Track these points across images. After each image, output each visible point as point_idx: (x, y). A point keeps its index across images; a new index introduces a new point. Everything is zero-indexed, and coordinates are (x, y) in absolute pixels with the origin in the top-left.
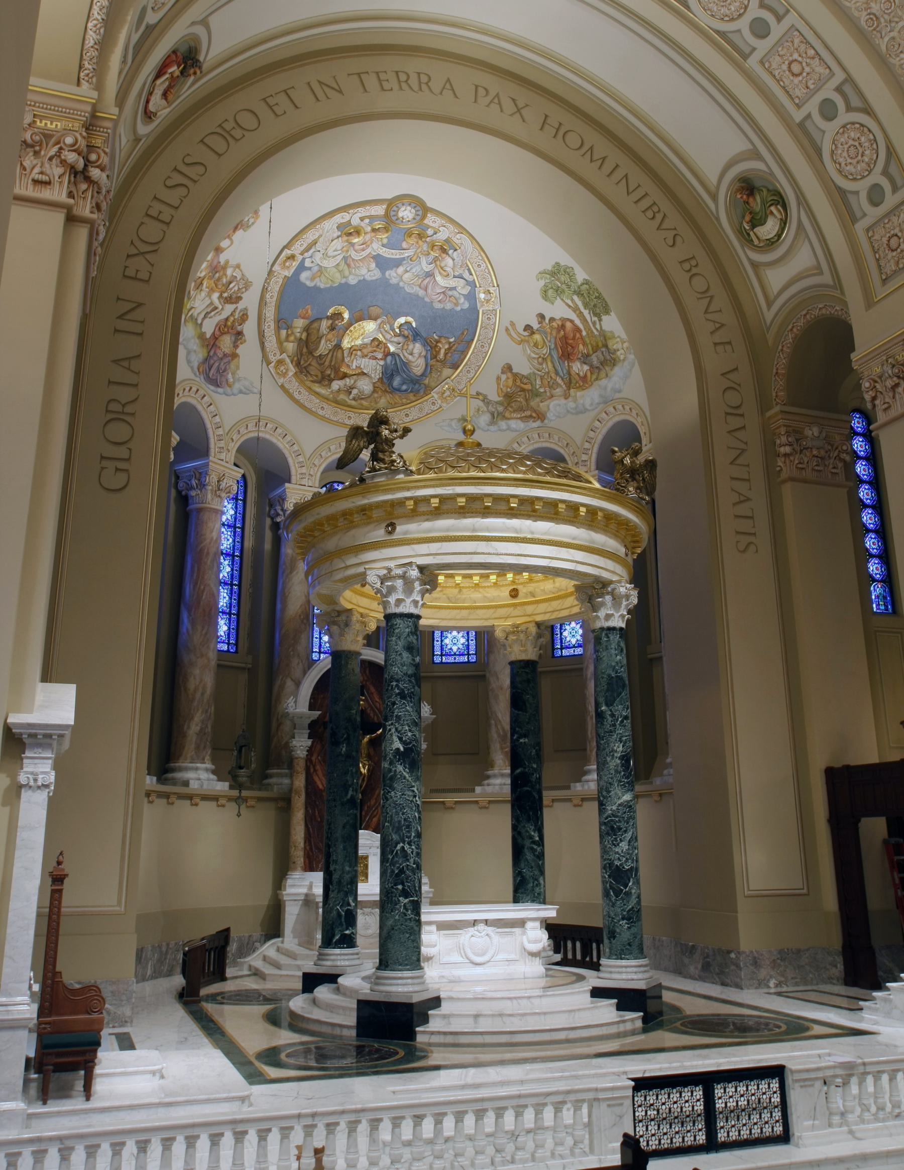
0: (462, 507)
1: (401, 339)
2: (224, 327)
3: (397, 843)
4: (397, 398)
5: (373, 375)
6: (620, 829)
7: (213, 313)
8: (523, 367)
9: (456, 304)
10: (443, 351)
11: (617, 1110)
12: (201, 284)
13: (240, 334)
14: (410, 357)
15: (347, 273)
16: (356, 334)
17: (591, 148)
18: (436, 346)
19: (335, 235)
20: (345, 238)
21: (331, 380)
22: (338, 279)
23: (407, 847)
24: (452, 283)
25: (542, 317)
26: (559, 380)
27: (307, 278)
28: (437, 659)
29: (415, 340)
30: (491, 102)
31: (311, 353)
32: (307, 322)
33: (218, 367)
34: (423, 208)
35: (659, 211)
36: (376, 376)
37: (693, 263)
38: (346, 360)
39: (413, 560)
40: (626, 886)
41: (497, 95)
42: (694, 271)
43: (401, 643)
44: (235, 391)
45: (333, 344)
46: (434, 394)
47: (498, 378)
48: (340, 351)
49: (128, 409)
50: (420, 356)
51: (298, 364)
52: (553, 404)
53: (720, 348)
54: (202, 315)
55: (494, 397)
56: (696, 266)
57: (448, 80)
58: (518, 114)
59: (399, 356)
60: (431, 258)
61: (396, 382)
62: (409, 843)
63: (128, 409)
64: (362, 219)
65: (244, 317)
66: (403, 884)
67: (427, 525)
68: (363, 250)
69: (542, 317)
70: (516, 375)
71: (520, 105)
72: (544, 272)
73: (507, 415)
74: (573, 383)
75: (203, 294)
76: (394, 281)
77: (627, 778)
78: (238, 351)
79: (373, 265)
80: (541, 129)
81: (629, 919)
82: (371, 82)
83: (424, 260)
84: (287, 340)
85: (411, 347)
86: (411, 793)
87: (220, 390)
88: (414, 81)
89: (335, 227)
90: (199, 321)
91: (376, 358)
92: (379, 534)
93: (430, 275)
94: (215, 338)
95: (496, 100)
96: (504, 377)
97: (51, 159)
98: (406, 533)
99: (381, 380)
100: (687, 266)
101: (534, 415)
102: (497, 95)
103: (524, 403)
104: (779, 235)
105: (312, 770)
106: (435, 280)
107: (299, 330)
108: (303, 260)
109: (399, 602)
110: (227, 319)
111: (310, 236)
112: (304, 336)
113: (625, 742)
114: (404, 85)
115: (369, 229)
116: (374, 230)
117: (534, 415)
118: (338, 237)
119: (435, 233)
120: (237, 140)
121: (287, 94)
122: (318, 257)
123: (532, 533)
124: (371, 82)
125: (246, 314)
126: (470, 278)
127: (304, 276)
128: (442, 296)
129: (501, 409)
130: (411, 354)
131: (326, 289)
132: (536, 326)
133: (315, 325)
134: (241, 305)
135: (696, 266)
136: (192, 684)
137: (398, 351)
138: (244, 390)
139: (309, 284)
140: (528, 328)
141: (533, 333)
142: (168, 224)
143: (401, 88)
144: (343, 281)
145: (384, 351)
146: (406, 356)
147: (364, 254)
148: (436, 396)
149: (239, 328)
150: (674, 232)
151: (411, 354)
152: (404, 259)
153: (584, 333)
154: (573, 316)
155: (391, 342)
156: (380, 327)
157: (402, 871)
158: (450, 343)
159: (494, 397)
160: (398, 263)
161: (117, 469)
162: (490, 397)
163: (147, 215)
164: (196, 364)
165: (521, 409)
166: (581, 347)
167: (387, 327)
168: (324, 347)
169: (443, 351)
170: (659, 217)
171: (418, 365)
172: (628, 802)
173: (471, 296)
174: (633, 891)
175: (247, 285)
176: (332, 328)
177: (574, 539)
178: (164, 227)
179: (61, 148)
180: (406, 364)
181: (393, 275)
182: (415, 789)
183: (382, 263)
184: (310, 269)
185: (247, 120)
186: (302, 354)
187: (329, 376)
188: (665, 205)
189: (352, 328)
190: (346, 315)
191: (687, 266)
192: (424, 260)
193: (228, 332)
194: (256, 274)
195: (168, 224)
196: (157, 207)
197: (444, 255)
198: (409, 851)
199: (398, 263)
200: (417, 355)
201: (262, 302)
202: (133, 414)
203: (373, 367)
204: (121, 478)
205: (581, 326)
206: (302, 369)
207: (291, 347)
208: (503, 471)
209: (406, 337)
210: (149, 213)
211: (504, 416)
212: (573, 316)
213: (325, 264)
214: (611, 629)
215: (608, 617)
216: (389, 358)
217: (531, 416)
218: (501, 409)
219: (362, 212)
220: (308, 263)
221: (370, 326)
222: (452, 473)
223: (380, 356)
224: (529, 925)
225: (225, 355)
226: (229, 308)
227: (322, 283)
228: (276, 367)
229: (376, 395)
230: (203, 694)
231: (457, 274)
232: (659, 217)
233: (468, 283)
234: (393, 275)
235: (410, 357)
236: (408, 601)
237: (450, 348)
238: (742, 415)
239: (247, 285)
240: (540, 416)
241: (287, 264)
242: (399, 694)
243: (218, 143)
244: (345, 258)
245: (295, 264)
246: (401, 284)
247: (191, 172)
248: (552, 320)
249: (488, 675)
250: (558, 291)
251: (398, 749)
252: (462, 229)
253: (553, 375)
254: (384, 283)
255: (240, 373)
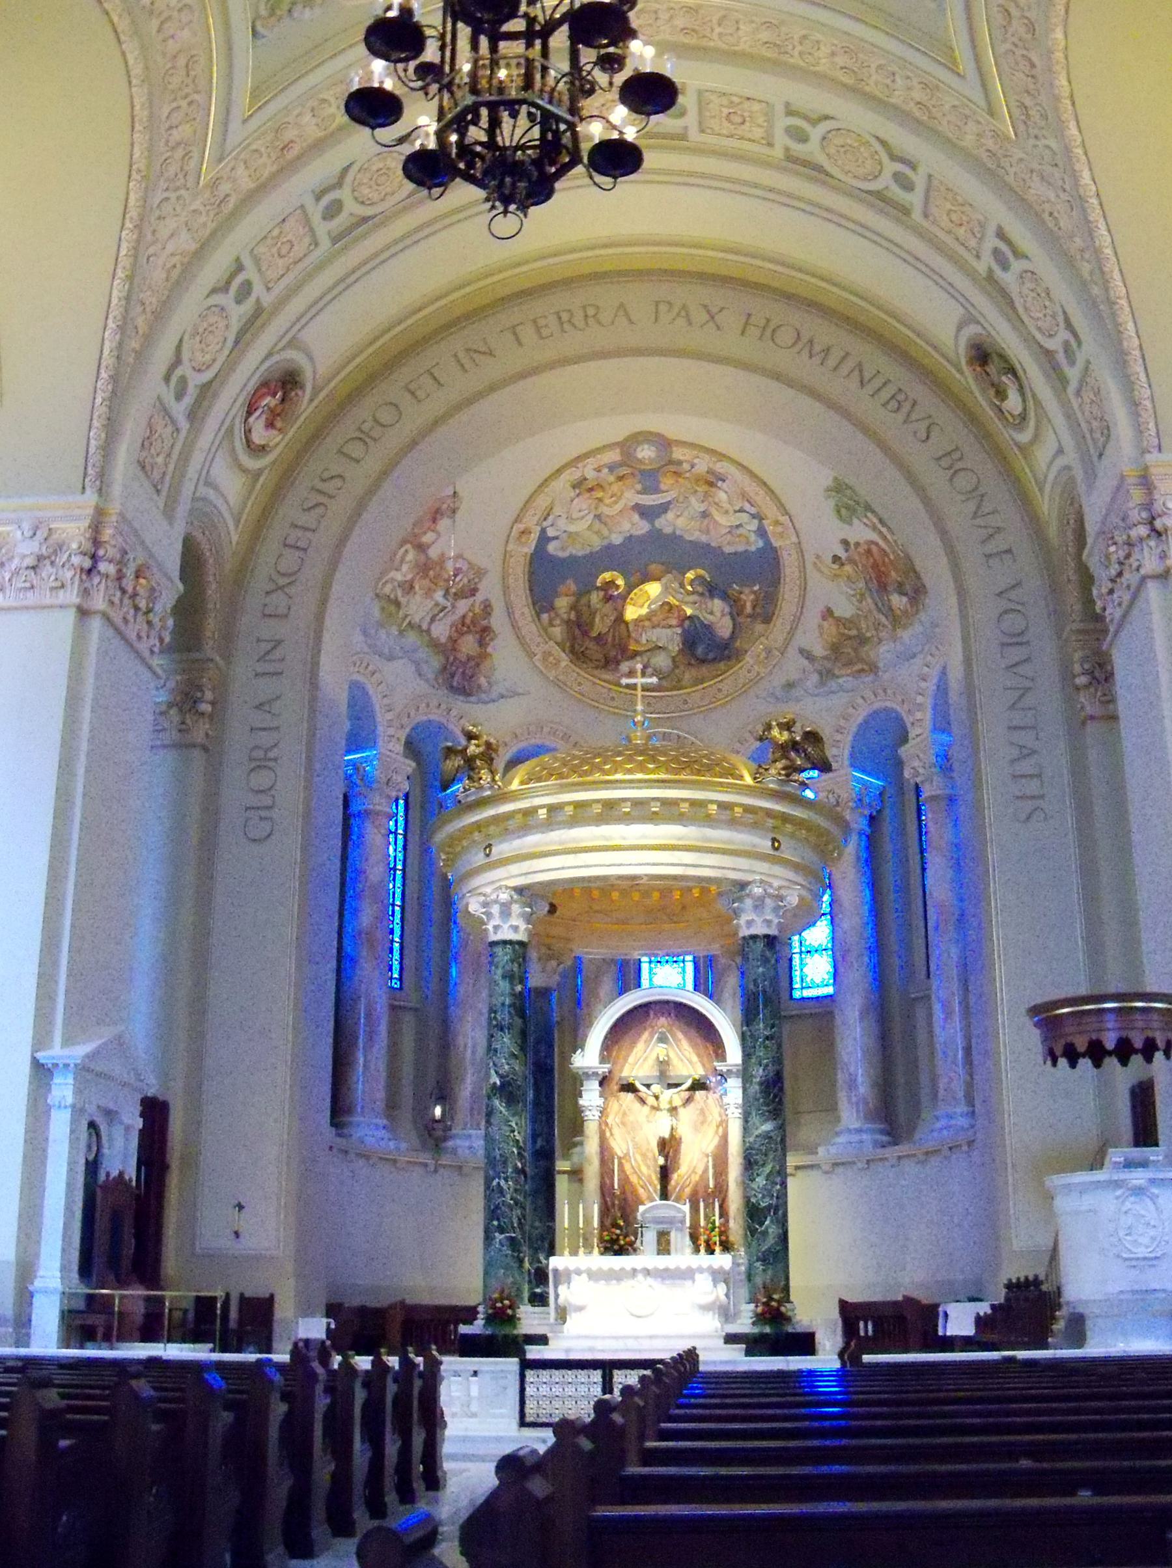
0: (600, 814)
1: (695, 598)
2: (463, 627)
3: (494, 1179)
4: (704, 670)
5: (670, 648)
6: (756, 1163)
7: (441, 615)
8: (845, 609)
9: (748, 543)
10: (749, 605)
11: (502, 1382)
12: (412, 587)
13: (486, 630)
14: (710, 617)
15: (605, 532)
16: (641, 601)
17: (811, 342)
18: (739, 599)
19: (572, 494)
20: (588, 495)
21: (618, 663)
22: (597, 543)
23: (502, 1183)
24: (735, 520)
25: (845, 543)
26: (883, 619)
27: (556, 549)
28: (797, 994)
29: (712, 596)
30: (678, 314)
31: (585, 633)
32: (572, 599)
33: (463, 673)
34: (664, 443)
35: (906, 399)
36: (675, 647)
37: (956, 455)
38: (633, 635)
39: (503, 883)
40: (761, 1224)
41: (684, 307)
42: (959, 465)
43: (500, 972)
44: (494, 695)
45: (612, 618)
46: (748, 659)
47: (820, 626)
48: (623, 626)
49: (271, 755)
50: (723, 615)
51: (573, 651)
52: (883, 649)
53: (994, 562)
54: (428, 619)
55: (819, 651)
56: (960, 459)
57: (622, 305)
58: (711, 324)
59: (698, 618)
60: (700, 495)
61: (700, 650)
62: (506, 1180)
63: (271, 755)
64: (598, 470)
65: (487, 608)
66: (498, 1219)
67: (517, 843)
68: (616, 502)
69: (845, 543)
70: (838, 620)
71: (714, 310)
72: (828, 490)
73: (836, 672)
74: (897, 620)
75: (418, 597)
76: (668, 530)
77: (768, 1105)
78: (489, 650)
79: (636, 517)
80: (743, 333)
81: (764, 1261)
82: (527, 334)
83: (693, 500)
84: (551, 625)
85: (710, 604)
86: (507, 1128)
87: (472, 699)
88: (578, 319)
89: (568, 485)
90: (425, 627)
91: (670, 626)
92: (479, 859)
93: (705, 515)
94: (453, 641)
95: (683, 313)
96: (825, 623)
97: (63, 566)
98: (500, 853)
99: (681, 651)
100: (945, 462)
101: (865, 667)
102: (684, 307)
103: (853, 654)
104: (1025, 409)
105: (608, 1134)
106: (716, 522)
107: (563, 610)
108: (543, 531)
109: (496, 928)
110: (464, 617)
111: (542, 502)
112: (573, 616)
113: (767, 1065)
114: (566, 326)
115: (612, 478)
116: (621, 478)
117: (865, 667)
118: (578, 495)
119: (692, 467)
120: (375, 440)
121: (515, 334)
122: (562, 523)
123: (624, 838)
124: (527, 334)
125: (489, 606)
126: (753, 510)
127: (551, 548)
128: (729, 536)
129: (829, 665)
130: (711, 613)
131: (584, 557)
132: (843, 555)
133: (584, 601)
134: (480, 597)
135: (960, 459)
136: (460, 1041)
137: (697, 613)
138: (505, 693)
139: (561, 554)
140: (836, 559)
141: (842, 564)
142: (305, 550)
143: (563, 331)
144: (605, 543)
145: (679, 616)
146: (707, 618)
147: (619, 507)
148: (751, 662)
149: (484, 623)
150: (926, 423)
151: (711, 613)
152: (669, 503)
153: (892, 557)
154: (874, 536)
155: (686, 603)
156: (666, 589)
157: (497, 1207)
158: (754, 593)
159: (819, 651)
160: (664, 508)
161: (261, 818)
162: (815, 653)
163: (285, 545)
164: (431, 676)
165: (849, 663)
166: (893, 573)
167: (675, 585)
168: (600, 626)
169: (749, 605)
170: (906, 407)
171: (724, 628)
172: (768, 1132)
173: (761, 532)
174: (770, 1231)
175: (480, 573)
176: (608, 599)
177: (679, 839)
178: (301, 554)
179: (70, 556)
180: (708, 628)
181: (667, 523)
182: (513, 1124)
183: (646, 513)
184: (556, 538)
185: (385, 416)
186: (575, 638)
187: (615, 657)
188: (918, 391)
189: (632, 595)
190: (620, 582)
191: (945, 462)
192: (693, 500)
193: (469, 632)
194: (487, 557)
195: (305, 550)
196: (294, 535)
197: (713, 489)
198: (505, 1187)
199: (664, 508)
200: (718, 614)
201: (506, 589)
202: (275, 760)
203: (670, 638)
204: (267, 826)
205: (887, 548)
206: (578, 656)
207: (558, 631)
208: (629, 771)
209: (702, 594)
210: (287, 542)
211: (834, 675)
212: (874, 536)
213: (572, 528)
214: (754, 937)
215: (750, 923)
216: (687, 623)
217: (862, 670)
218: (829, 665)
219: (591, 463)
220: (551, 533)
221: (653, 589)
222: (574, 779)
223: (674, 622)
224: (698, 1276)
225: (469, 658)
226: (463, 606)
227: (578, 551)
228: (545, 659)
229: (677, 671)
230: (473, 1053)
231: (737, 508)
232: (906, 407)
233: (753, 516)
234: (660, 523)
235: (710, 617)
236: (506, 926)
237: (757, 600)
238: (1028, 643)
239: (480, 573)
240: (873, 668)
241: (523, 540)
242: (496, 1026)
243: (356, 450)
244: (598, 517)
245: (534, 537)
246: (678, 533)
247: (329, 487)
248: (857, 544)
249: (836, 1012)
250: (852, 511)
251: (495, 1083)
252: (722, 456)
253: (875, 612)
254: (655, 536)
255: (498, 675)
